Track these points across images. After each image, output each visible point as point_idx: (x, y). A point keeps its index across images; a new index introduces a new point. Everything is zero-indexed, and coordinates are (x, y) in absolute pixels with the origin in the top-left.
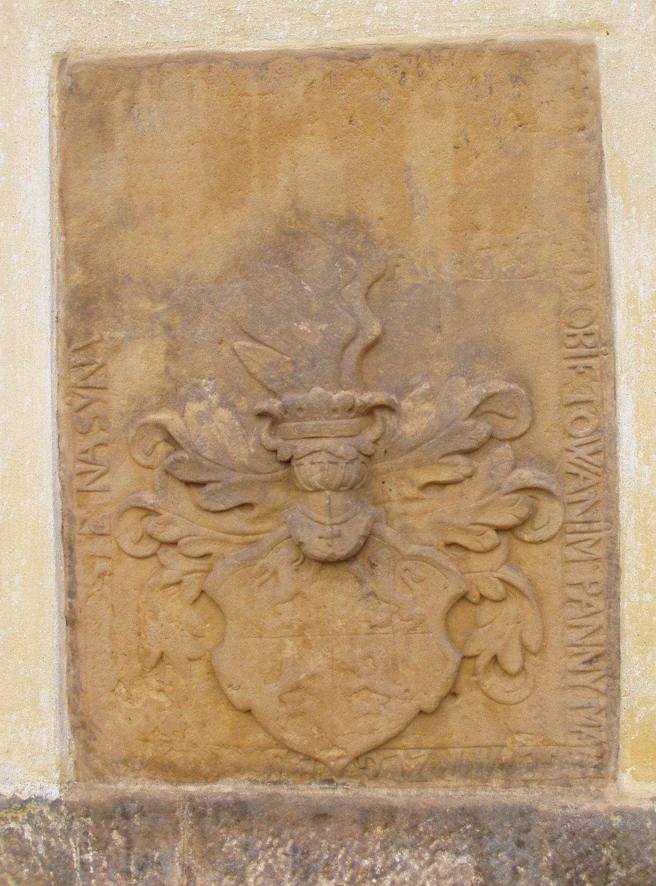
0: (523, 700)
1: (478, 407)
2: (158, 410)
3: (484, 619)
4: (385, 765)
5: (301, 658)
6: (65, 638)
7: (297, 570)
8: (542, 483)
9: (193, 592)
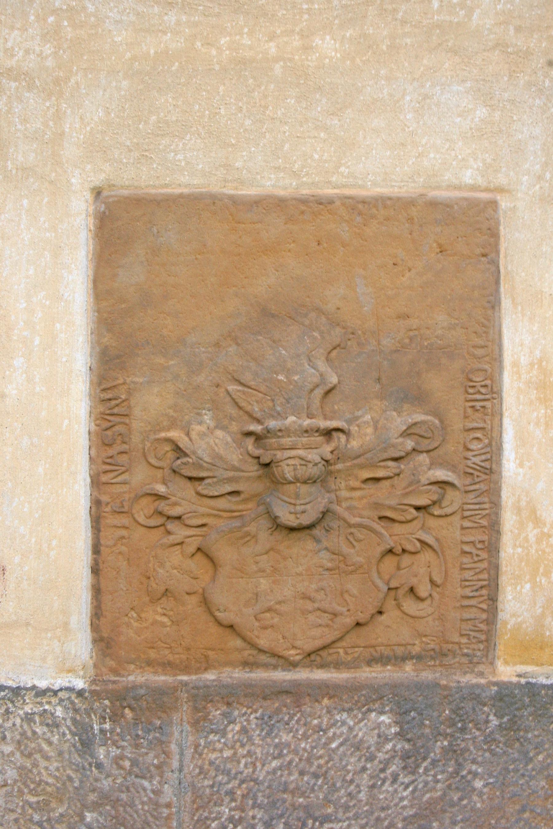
0: (429, 615)
1: (405, 431)
2: (168, 430)
3: (403, 565)
4: (330, 659)
5: (272, 591)
6: (90, 581)
7: (271, 534)
8: (450, 479)
9: (192, 549)
